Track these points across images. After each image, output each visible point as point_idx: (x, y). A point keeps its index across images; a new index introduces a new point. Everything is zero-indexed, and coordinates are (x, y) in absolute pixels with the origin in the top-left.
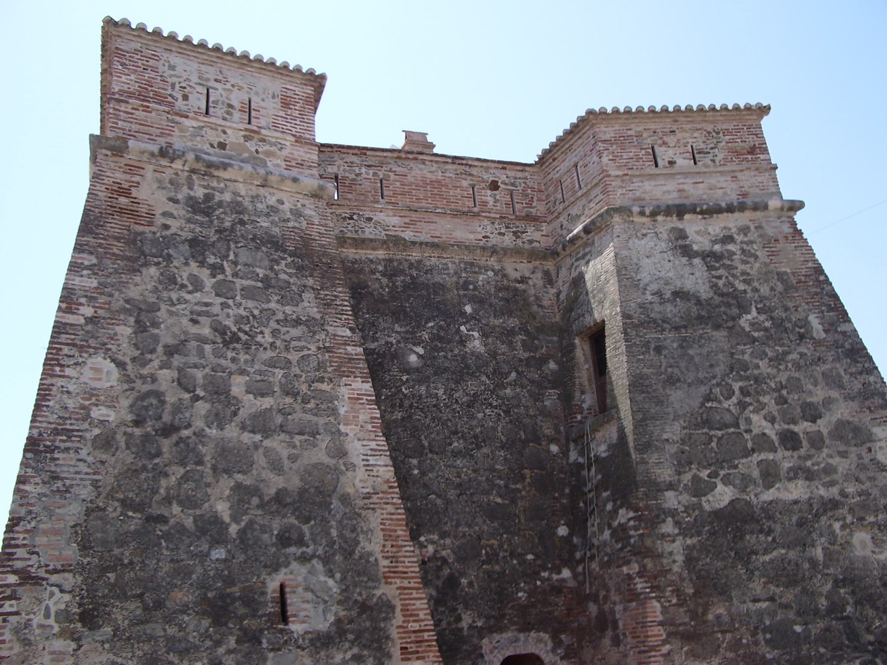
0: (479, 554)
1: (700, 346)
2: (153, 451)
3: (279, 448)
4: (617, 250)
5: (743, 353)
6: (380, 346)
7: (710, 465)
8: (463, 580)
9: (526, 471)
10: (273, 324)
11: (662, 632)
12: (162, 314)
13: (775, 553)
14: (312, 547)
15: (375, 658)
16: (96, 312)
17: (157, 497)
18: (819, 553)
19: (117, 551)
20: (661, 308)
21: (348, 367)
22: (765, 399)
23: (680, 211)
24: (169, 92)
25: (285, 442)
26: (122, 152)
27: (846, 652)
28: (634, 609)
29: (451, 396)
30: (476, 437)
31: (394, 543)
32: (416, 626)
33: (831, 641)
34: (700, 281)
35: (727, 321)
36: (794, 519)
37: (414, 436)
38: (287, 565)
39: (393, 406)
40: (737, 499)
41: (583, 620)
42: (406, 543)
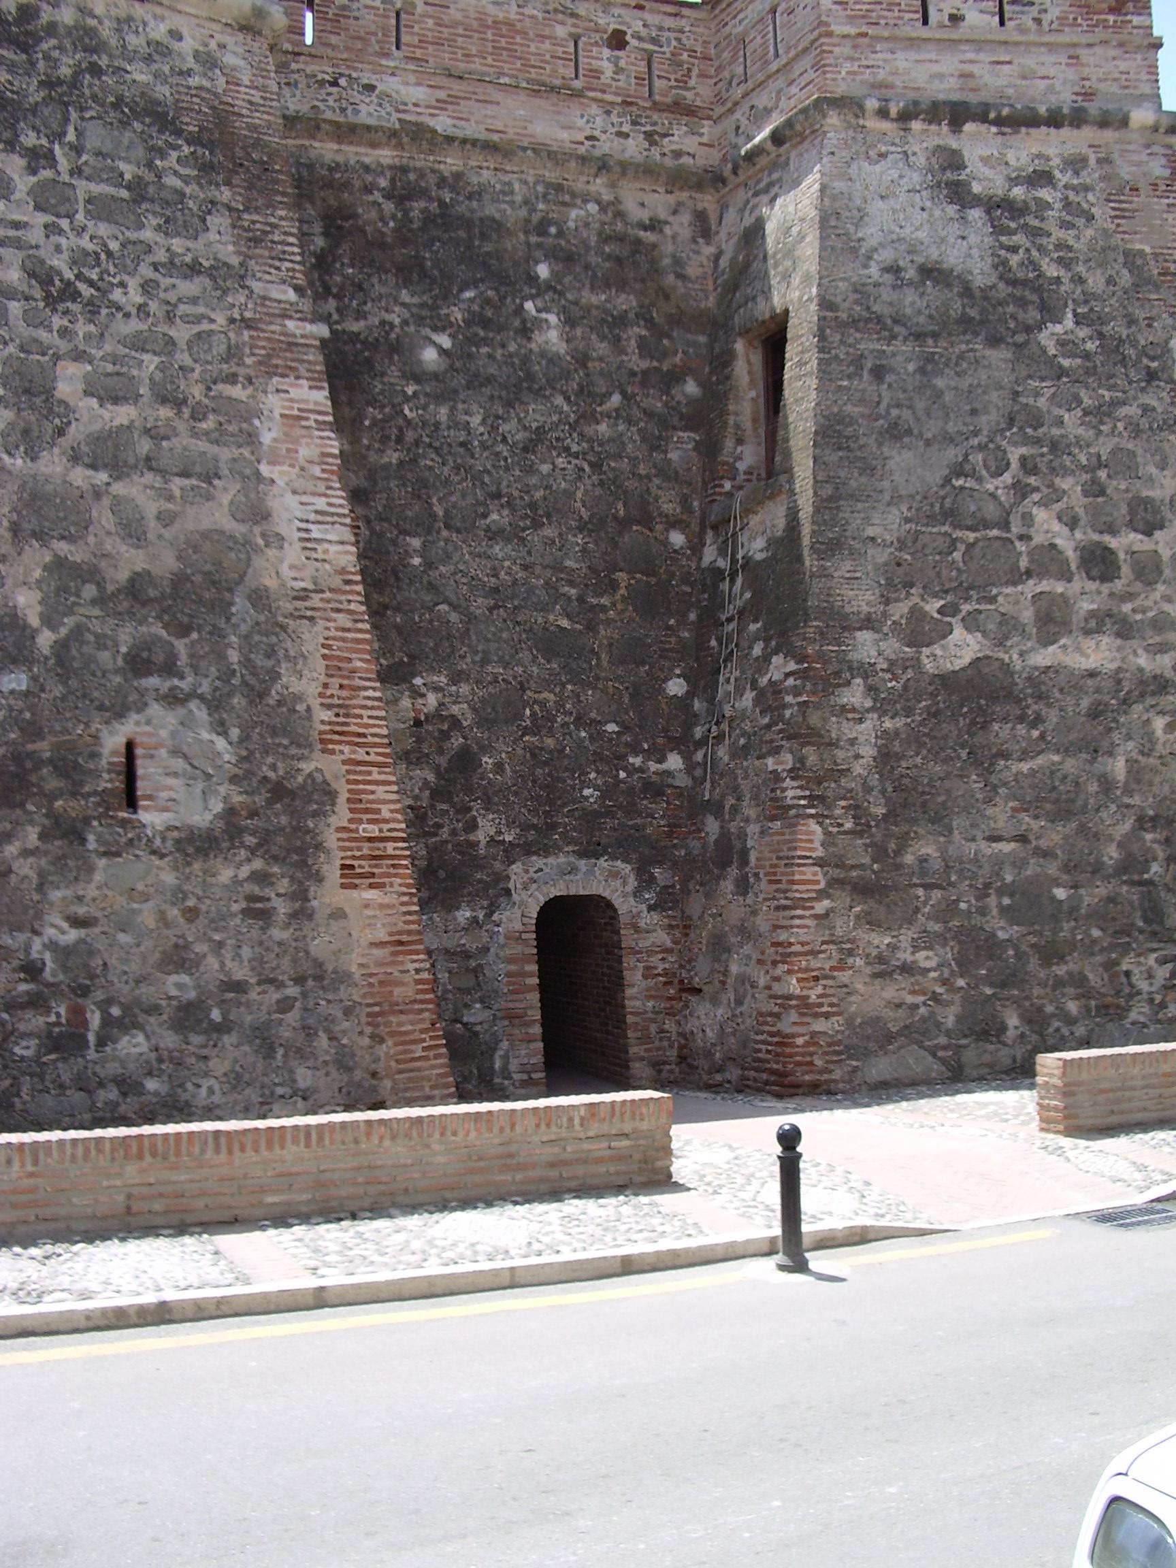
1: (957, 374)
3: (141, 499)
4: (826, 180)
5: (1037, 394)
6: (369, 328)
7: (946, 592)
8: (485, 759)
9: (621, 576)
10: (146, 271)
11: (820, 877)
13: (1040, 760)
14: (190, 679)
15: (292, 878)
18: (1118, 767)
20: (895, 296)
21: (286, 359)
22: (1065, 484)
25: (152, 487)
27: (1136, 940)
28: (777, 833)
30: (533, 506)
31: (345, 682)
32: (373, 830)
33: (1114, 919)
34: (975, 252)
35: (1014, 333)
36: (1085, 703)
37: (419, 497)
38: (141, 707)
39: (385, 439)
40: (987, 657)
42: (368, 684)
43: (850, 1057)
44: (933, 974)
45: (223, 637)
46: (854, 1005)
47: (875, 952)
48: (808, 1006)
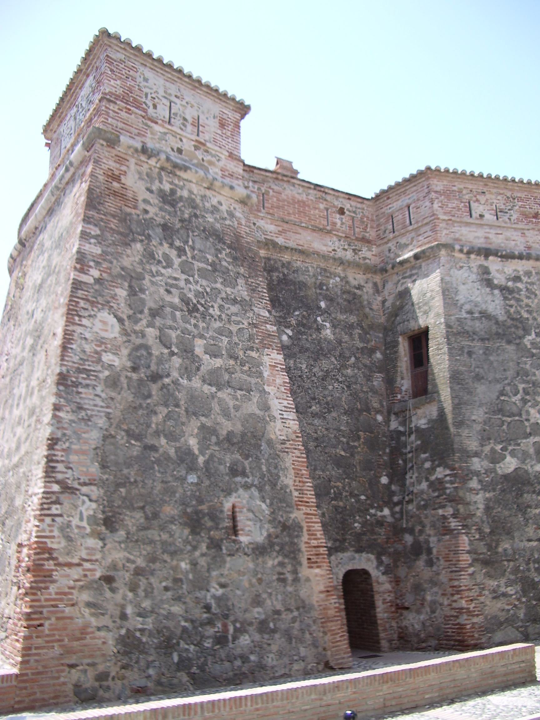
0: (329, 493)
2: (146, 393)
3: (227, 400)
7: (502, 442)
9: (361, 433)
10: (219, 301)
11: (469, 558)
12: (146, 282)
14: (251, 478)
15: (292, 564)
16: (101, 275)
17: (150, 431)
19: (125, 471)
21: (268, 341)
23: (487, 253)
24: (144, 100)
26: (114, 144)
29: (311, 370)
30: (327, 403)
34: (498, 307)
38: (236, 490)
40: (519, 468)
41: (399, 547)
43: (488, 633)
44: (514, 597)
45: (260, 460)
46: (487, 611)
47: (492, 589)
48: (470, 612)
